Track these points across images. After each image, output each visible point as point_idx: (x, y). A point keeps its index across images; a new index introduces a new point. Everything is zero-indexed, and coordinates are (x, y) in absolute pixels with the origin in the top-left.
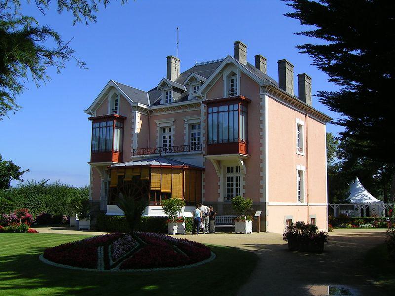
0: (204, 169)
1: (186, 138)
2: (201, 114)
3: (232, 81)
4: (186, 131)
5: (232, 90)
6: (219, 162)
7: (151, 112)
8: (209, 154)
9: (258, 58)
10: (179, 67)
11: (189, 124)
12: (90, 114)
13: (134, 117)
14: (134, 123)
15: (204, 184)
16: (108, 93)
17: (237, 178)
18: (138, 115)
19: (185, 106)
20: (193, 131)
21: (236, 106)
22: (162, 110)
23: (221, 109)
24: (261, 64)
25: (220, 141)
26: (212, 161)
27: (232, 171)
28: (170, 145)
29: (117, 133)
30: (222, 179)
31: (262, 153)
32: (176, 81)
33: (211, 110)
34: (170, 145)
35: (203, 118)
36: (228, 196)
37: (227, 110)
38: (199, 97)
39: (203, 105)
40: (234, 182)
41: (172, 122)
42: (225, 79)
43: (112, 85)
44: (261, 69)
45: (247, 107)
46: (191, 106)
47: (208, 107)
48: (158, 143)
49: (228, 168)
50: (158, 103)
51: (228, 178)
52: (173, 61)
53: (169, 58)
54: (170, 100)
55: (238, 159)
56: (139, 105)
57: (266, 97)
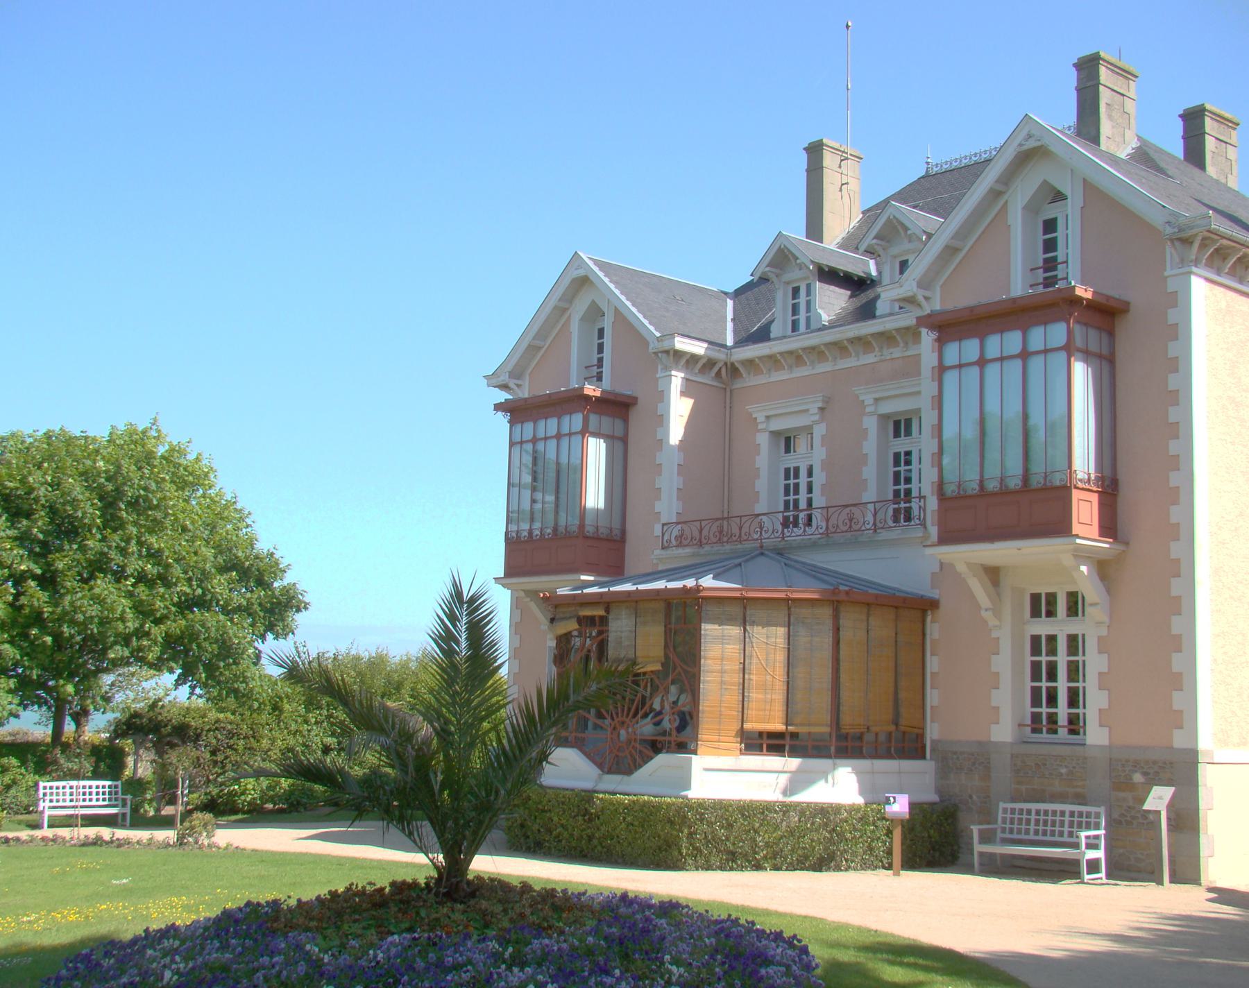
0: (933, 604)
1: (870, 472)
2: (919, 374)
3: (1050, 226)
4: (870, 446)
5: (1050, 265)
6: (993, 574)
7: (733, 370)
8: (947, 538)
9: (1193, 120)
10: (854, 185)
11: (772, 432)
12: (504, 387)
13: (662, 397)
14: (661, 420)
15: (932, 664)
16: (571, 301)
17: (1073, 641)
18: (677, 379)
19: (862, 343)
20: (791, 461)
21: (1057, 333)
22: (773, 361)
23: (994, 345)
24: (1210, 143)
25: (992, 486)
26: (961, 568)
27: (1050, 613)
28: (810, 502)
29: (596, 452)
30: (1006, 646)
31: (1182, 532)
32: (844, 245)
33: (952, 353)
34: (810, 502)
35: (928, 387)
36: (1036, 718)
37: (974, 356)
38: (911, 300)
39: (928, 338)
40: (1062, 659)
41: (814, 408)
42: (1016, 218)
43: (581, 272)
44: (1211, 170)
45: (1111, 334)
46: (887, 338)
47: (941, 342)
48: (763, 495)
49: (1035, 598)
50: (763, 335)
51: (1036, 640)
52: (829, 160)
53: (815, 151)
54: (808, 319)
55: (1068, 560)
56: (682, 344)
57: (1194, 280)
